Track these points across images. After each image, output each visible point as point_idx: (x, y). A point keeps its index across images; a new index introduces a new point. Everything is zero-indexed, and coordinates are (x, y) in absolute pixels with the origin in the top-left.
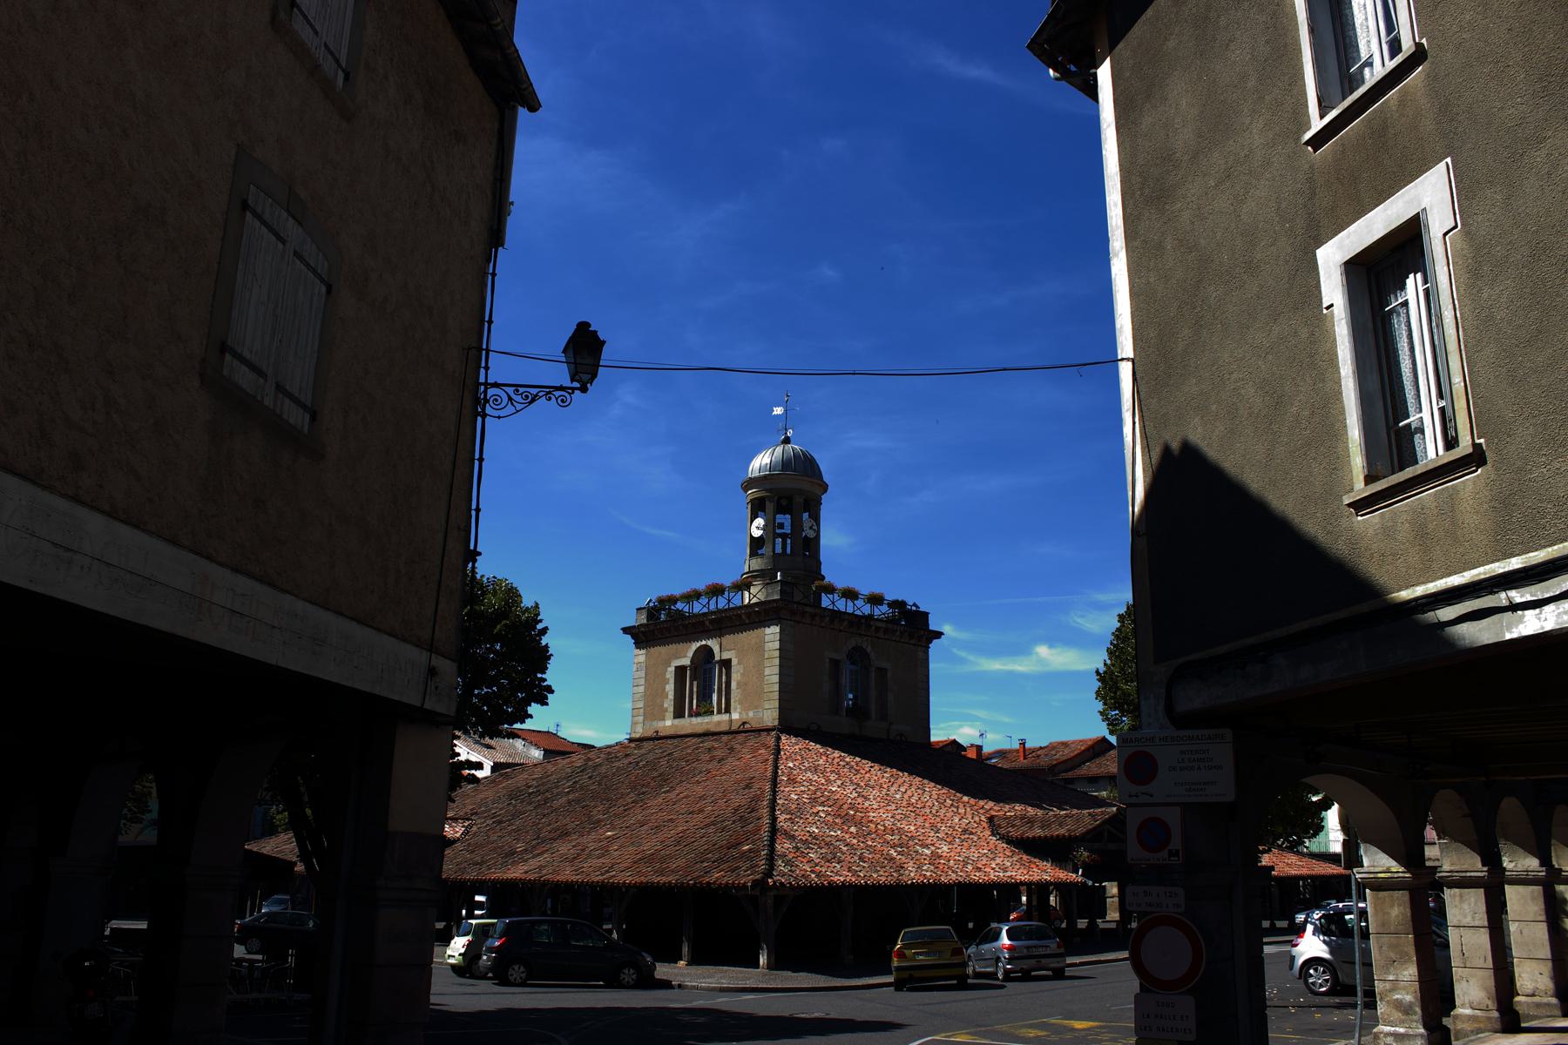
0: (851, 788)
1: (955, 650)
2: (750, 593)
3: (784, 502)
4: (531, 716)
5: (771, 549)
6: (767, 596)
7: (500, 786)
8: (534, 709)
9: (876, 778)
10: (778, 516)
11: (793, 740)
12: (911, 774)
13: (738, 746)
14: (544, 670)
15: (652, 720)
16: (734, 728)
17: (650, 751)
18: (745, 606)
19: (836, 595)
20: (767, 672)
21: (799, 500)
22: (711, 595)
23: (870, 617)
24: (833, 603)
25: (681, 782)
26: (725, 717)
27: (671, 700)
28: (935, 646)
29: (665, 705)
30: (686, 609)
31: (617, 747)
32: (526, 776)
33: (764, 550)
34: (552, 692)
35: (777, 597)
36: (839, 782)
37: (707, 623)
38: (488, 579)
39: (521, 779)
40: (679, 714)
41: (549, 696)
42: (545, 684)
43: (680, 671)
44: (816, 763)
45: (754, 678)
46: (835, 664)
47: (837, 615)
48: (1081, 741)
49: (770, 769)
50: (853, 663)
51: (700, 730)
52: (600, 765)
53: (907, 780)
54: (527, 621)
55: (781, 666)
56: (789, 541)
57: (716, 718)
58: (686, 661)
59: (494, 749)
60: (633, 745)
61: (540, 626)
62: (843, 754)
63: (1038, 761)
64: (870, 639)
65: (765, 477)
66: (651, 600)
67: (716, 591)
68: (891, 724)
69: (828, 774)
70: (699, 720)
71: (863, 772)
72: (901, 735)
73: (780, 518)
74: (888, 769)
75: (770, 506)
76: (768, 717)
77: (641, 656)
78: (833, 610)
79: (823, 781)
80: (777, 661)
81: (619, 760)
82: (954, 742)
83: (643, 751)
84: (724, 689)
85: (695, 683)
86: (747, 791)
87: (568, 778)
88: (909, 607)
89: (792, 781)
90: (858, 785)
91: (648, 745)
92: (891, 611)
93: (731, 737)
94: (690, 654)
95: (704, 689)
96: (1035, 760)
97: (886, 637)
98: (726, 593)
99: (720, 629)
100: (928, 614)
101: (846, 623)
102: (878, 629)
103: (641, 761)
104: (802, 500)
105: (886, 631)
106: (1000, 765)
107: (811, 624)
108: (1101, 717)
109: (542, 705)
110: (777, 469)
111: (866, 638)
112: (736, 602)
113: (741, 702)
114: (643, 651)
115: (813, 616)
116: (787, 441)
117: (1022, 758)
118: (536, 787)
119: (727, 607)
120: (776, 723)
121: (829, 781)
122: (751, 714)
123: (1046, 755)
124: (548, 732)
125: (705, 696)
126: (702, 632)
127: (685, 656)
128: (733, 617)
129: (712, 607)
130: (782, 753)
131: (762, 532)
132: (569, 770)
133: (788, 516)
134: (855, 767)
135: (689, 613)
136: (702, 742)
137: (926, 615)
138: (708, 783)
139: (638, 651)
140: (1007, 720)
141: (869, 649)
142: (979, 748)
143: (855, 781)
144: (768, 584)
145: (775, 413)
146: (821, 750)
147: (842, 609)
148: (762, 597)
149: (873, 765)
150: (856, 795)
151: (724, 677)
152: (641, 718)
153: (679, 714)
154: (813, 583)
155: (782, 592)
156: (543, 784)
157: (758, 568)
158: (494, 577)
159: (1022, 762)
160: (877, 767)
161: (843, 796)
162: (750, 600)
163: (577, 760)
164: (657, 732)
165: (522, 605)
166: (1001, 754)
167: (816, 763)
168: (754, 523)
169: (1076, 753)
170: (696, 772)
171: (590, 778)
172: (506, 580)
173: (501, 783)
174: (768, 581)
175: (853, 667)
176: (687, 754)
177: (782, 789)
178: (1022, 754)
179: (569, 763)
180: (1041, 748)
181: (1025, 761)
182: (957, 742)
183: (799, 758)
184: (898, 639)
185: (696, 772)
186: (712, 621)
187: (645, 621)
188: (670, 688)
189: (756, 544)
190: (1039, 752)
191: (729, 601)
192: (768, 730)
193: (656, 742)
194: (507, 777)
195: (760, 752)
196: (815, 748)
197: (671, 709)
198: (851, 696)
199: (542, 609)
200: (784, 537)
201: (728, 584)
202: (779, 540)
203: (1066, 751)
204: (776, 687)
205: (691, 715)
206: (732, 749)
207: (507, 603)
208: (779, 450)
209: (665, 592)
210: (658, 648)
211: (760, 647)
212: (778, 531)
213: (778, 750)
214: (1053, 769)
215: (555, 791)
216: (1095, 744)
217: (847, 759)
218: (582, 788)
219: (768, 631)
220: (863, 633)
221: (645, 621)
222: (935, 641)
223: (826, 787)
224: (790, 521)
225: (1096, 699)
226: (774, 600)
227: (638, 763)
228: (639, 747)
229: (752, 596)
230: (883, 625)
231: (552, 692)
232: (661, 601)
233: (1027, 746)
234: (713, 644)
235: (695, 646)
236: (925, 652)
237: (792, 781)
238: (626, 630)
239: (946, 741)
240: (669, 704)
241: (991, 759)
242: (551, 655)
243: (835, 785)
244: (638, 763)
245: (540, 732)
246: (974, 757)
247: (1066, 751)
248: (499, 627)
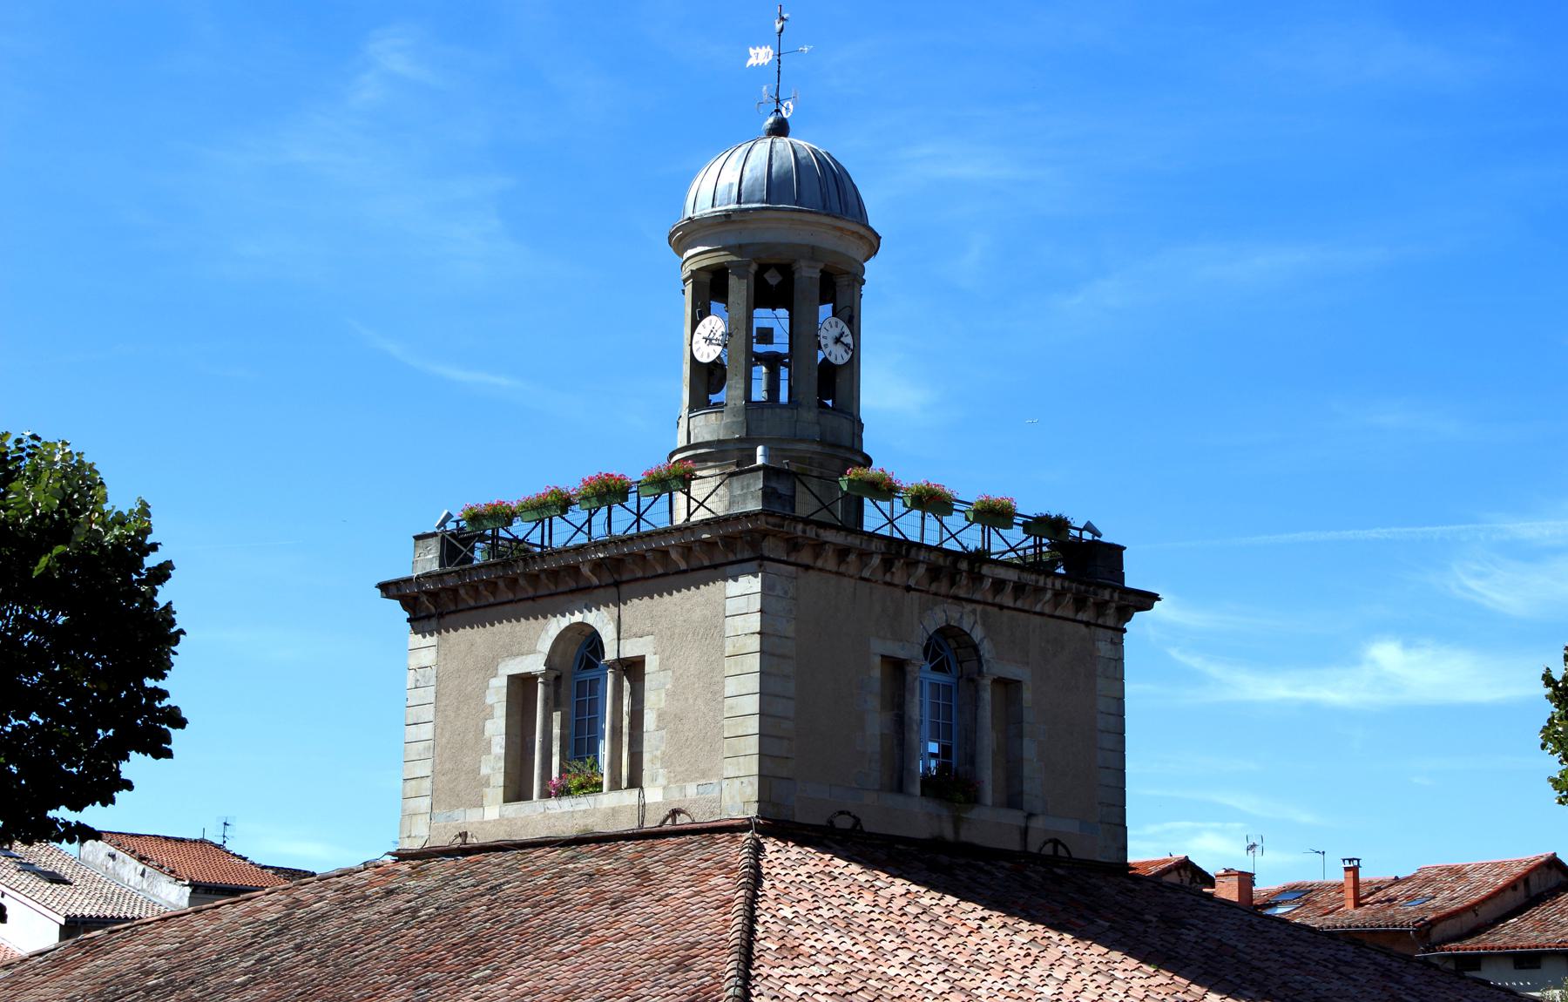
0: (935, 969)
1: (1174, 653)
2: (689, 498)
3: (773, 278)
4: (129, 785)
5: (740, 392)
6: (731, 504)
7: (76, 973)
8: (135, 766)
9: (994, 946)
10: (758, 312)
11: (794, 851)
12: (1080, 936)
13: (659, 869)
14: (160, 668)
15: (452, 807)
16: (651, 823)
17: (446, 882)
18: (678, 529)
19: (898, 504)
20: (731, 687)
21: (808, 273)
22: (594, 503)
23: (980, 557)
24: (891, 521)
25: (520, 955)
26: (629, 797)
27: (497, 757)
28: (1139, 626)
29: (485, 771)
30: (535, 538)
31: (365, 874)
32: (142, 947)
33: (730, 394)
34: (181, 723)
35: (754, 505)
36: (904, 956)
37: (585, 570)
38: (19, 441)
39: (125, 956)
40: (517, 790)
41: (175, 733)
42: (165, 703)
43: (521, 686)
44: (850, 909)
45: (700, 702)
46: (896, 668)
47: (899, 550)
48: (1496, 865)
49: (737, 922)
50: (938, 668)
51: (569, 830)
52: (324, 917)
53: (1070, 951)
54: (118, 546)
55: (763, 673)
56: (784, 373)
57: (608, 800)
58: (535, 663)
59: (66, 882)
60: (404, 867)
61: (151, 561)
62: (914, 888)
63: (1390, 912)
64: (979, 608)
65: (728, 217)
66: (449, 516)
67: (609, 492)
68: (1030, 816)
69: (878, 937)
70: (566, 804)
71: (964, 931)
72: (1056, 842)
73: (764, 317)
74: (1025, 925)
75: (738, 288)
76: (732, 798)
77: (424, 650)
78: (890, 539)
79: (866, 953)
80: (754, 662)
81: (371, 905)
82: (1185, 865)
83: (428, 882)
84: (626, 730)
85: (557, 716)
86: (679, 976)
87: (243, 950)
88: (1077, 533)
89: (790, 952)
90: (951, 962)
91: (440, 869)
92: (1031, 541)
93: (642, 845)
94: (545, 645)
95: (579, 724)
96: (1383, 910)
97: (1019, 604)
98: (632, 498)
99: (617, 584)
100: (1120, 549)
101: (921, 570)
102: (999, 585)
103: (424, 905)
104: (817, 275)
105: (1019, 589)
106: (1297, 921)
107: (837, 573)
108: (1556, 793)
109: (156, 756)
110: (757, 198)
111: (969, 607)
112: (657, 518)
113: (666, 762)
114: (431, 640)
115: (843, 553)
116: (780, 128)
117: (1350, 904)
118: (165, 973)
119: (633, 531)
120: (752, 811)
121: (877, 951)
122: (691, 790)
123: (1410, 898)
124: (202, 841)
125: (580, 745)
126: (572, 591)
127: (533, 651)
128: (649, 555)
129: (599, 531)
130: (766, 884)
131: (719, 349)
132: (247, 931)
133: (783, 313)
134: (943, 919)
135: (542, 546)
136: (572, 859)
137: (1116, 551)
138: (586, 957)
139: (417, 640)
140: (1306, 818)
141: (977, 634)
142: (1246, 879)
143: (944, 953)
144: (731, 475)
145: (752, 61)
146: (862, 878)
147: (914, 537)
148: (718, 506)
149: (986, 913)
150: (947, 986)
151: (626, 701)
152: (425, 803)
153: (517, 790)
154: (842, 474)
155: (768, 495)
156: (181, 966)
157: (708, 438)
158: (34, 437)
159: (1351, 915)
160: (997, 918)
161: (914, 988)
162: (689, 515)
163: (268, 907)
164: (464, 835)
165: (107, 507)
166: (1301, 893)
167: (850, 909)
168: (700, 328)
169: (1484, 893)
170: (559, 932)
171: (298, 948)
172: (65, 443)
173: (78, 964)
174: (734, 469)
175: (939, 678)
176: (536, 887)
177: (764, 971)
178: (1349, 893)
179: (248, 914)
180: (1397, 880)
181: (1357, 911)
182: (1193, 865)
183: (807, 896)
184: (1047, 610)
185: (559, 932)
186: (598, 565)
187: (435, 567)
188: (496, 728)
189: (707, 379)
190: (1392, 891)
191: (639, 516)
192: (732, 829)
193: (462, 860)
194: (94, 949)
195: (713, 881)
196: (847, 871)
197: (499, 779)
198: (933, 747)
199: (155, 521)
200: (773, 362)
201: (635, 474)
202: (761, 371)
203: (1460, 889)
204: (753, 725)
205: (545, 795)
206: (644, 875)
207: (66, 501)
208: (761, 149)
209: (483, 498)
210: (466, 634)
211: (714, 630)
212: (759, 348)
213: (756, 878)
214: (1425, 931)
215: (212, 982)
216: (1531, 871)
217: (926, 901)
218: (277, 975)
219: (732, 587)
220: (962, 594)
221: (435, 567)
222: (1137, 616)
223: (872, 967)
224: (786, 324)
225: (1543, 746)
226: (747, 515)
227: (415, 910)
228: (417, 873)
229: (694, 505)
230: (1012, 575)
231: (181, 723)
232: (475, 518)
233: (1363, 876)
234: (600, 620)
235: (557, 625)
236: (1112, 642)
237: (790, 952)
238: (387, 589)
239: (1165, 861)
240: (493, 766)
241: (1275, 905)
242: (181, 632)
243: (894, 961)
244: (415, 910)
245: (183, 840)
246: (1234, 897)
247: (1460, 889)
248: (44, 561)
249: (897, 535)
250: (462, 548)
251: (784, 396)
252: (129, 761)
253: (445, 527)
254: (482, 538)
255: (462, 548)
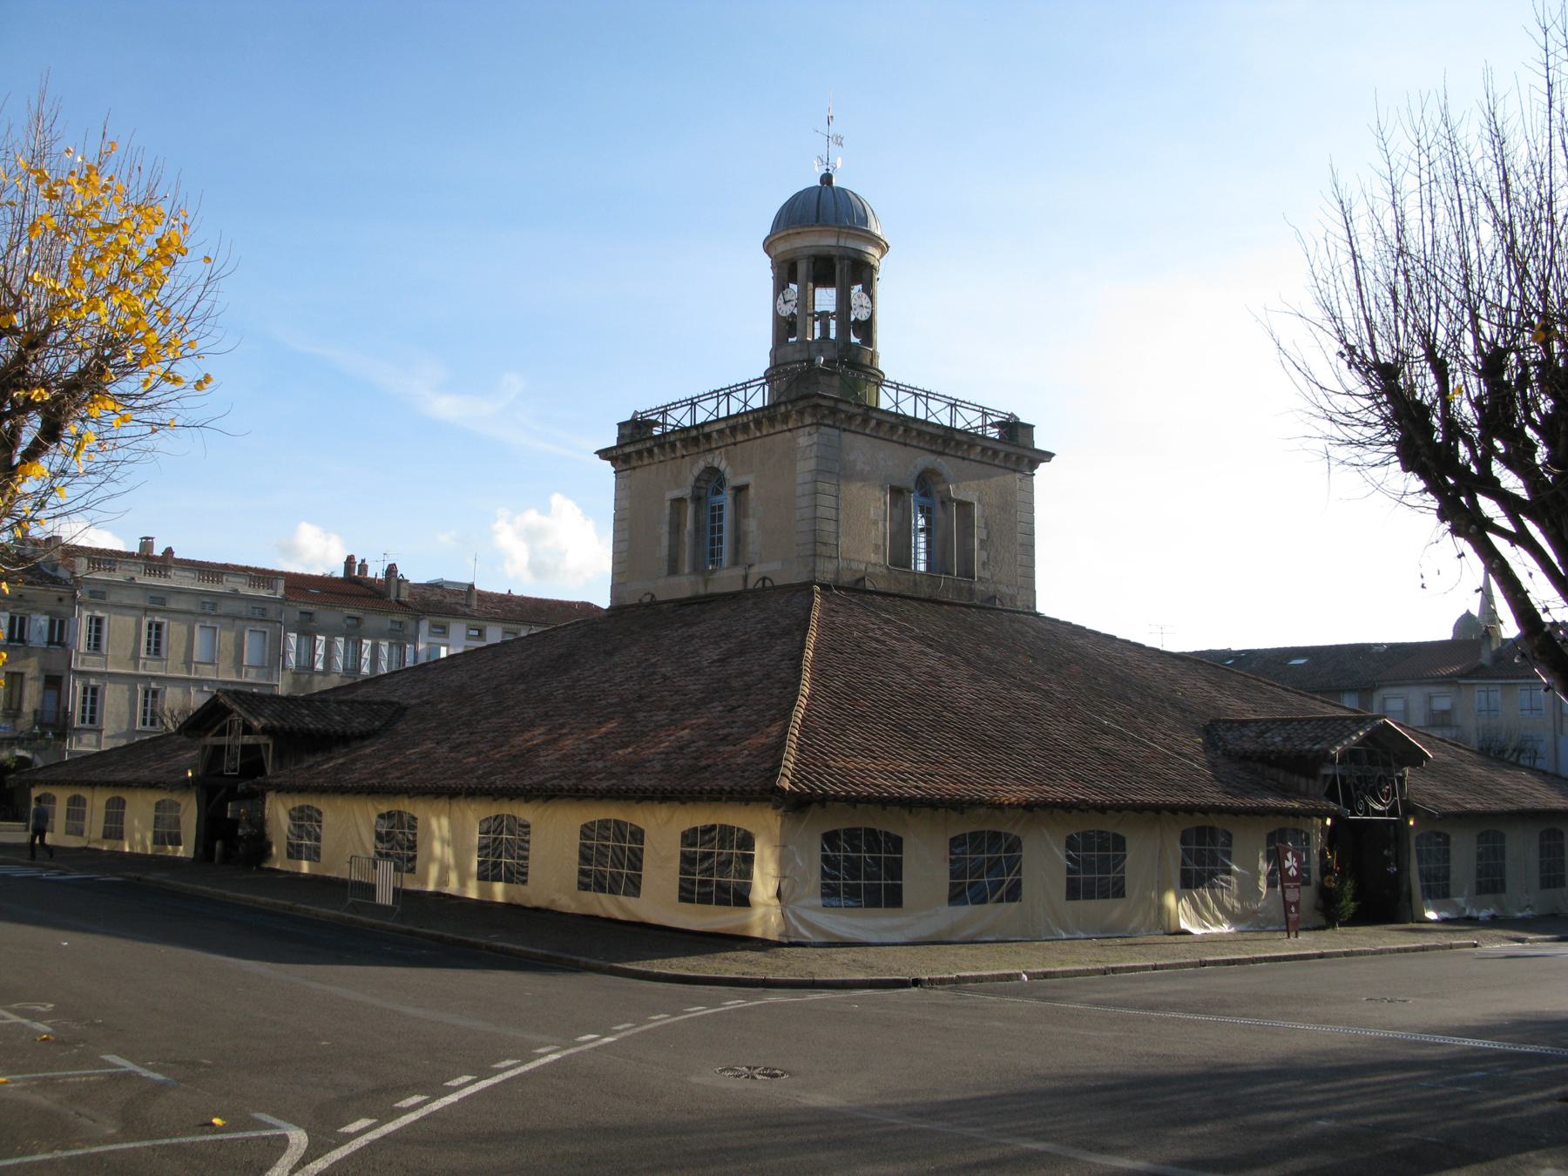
24: (897, 404)
222: (1042, 465)
249: (899, 412)
250: (693, 849)
251: (833, 335)
252: (604, 454)
253: (1366, 704)
254: (83, 262)
255: (693, 849)
